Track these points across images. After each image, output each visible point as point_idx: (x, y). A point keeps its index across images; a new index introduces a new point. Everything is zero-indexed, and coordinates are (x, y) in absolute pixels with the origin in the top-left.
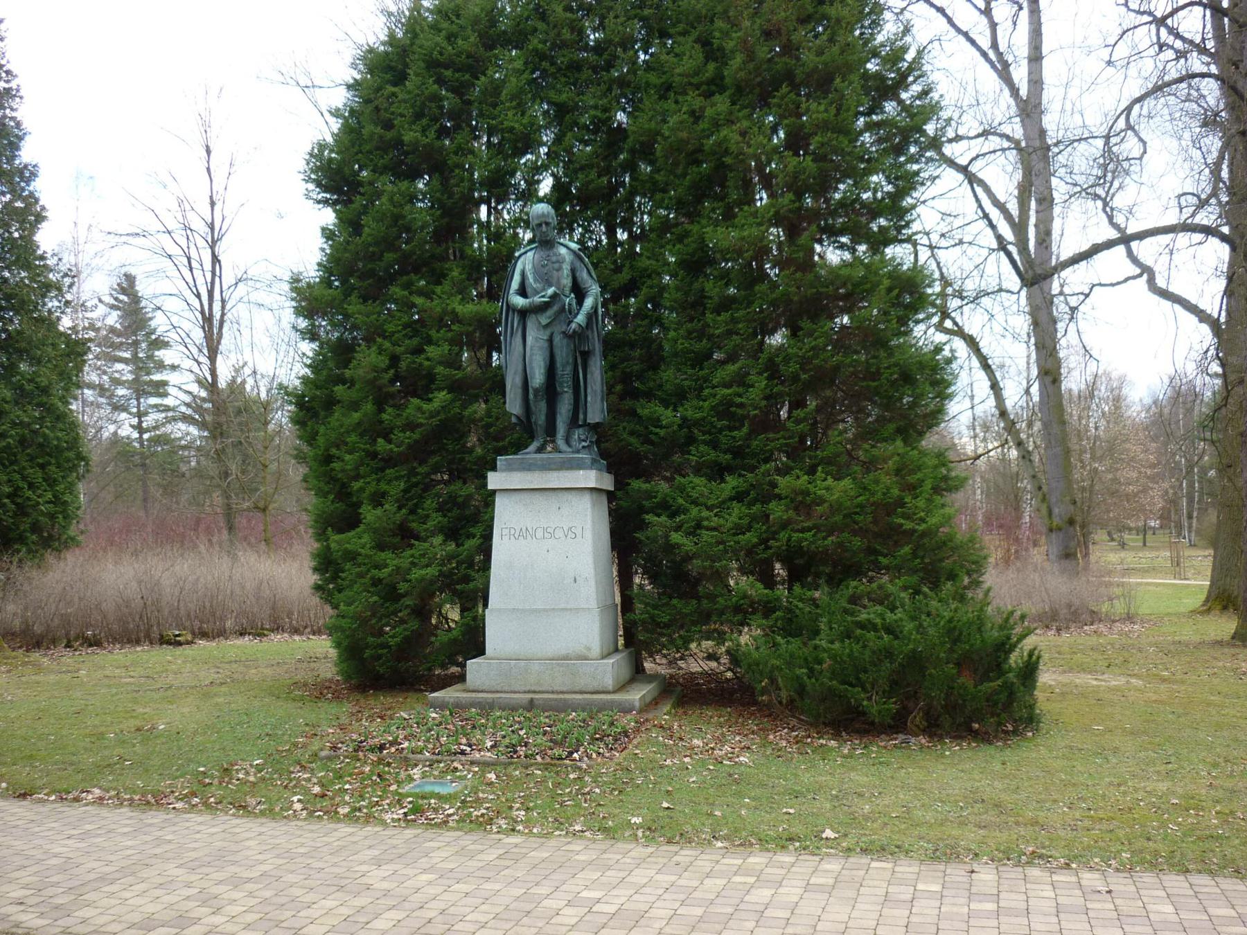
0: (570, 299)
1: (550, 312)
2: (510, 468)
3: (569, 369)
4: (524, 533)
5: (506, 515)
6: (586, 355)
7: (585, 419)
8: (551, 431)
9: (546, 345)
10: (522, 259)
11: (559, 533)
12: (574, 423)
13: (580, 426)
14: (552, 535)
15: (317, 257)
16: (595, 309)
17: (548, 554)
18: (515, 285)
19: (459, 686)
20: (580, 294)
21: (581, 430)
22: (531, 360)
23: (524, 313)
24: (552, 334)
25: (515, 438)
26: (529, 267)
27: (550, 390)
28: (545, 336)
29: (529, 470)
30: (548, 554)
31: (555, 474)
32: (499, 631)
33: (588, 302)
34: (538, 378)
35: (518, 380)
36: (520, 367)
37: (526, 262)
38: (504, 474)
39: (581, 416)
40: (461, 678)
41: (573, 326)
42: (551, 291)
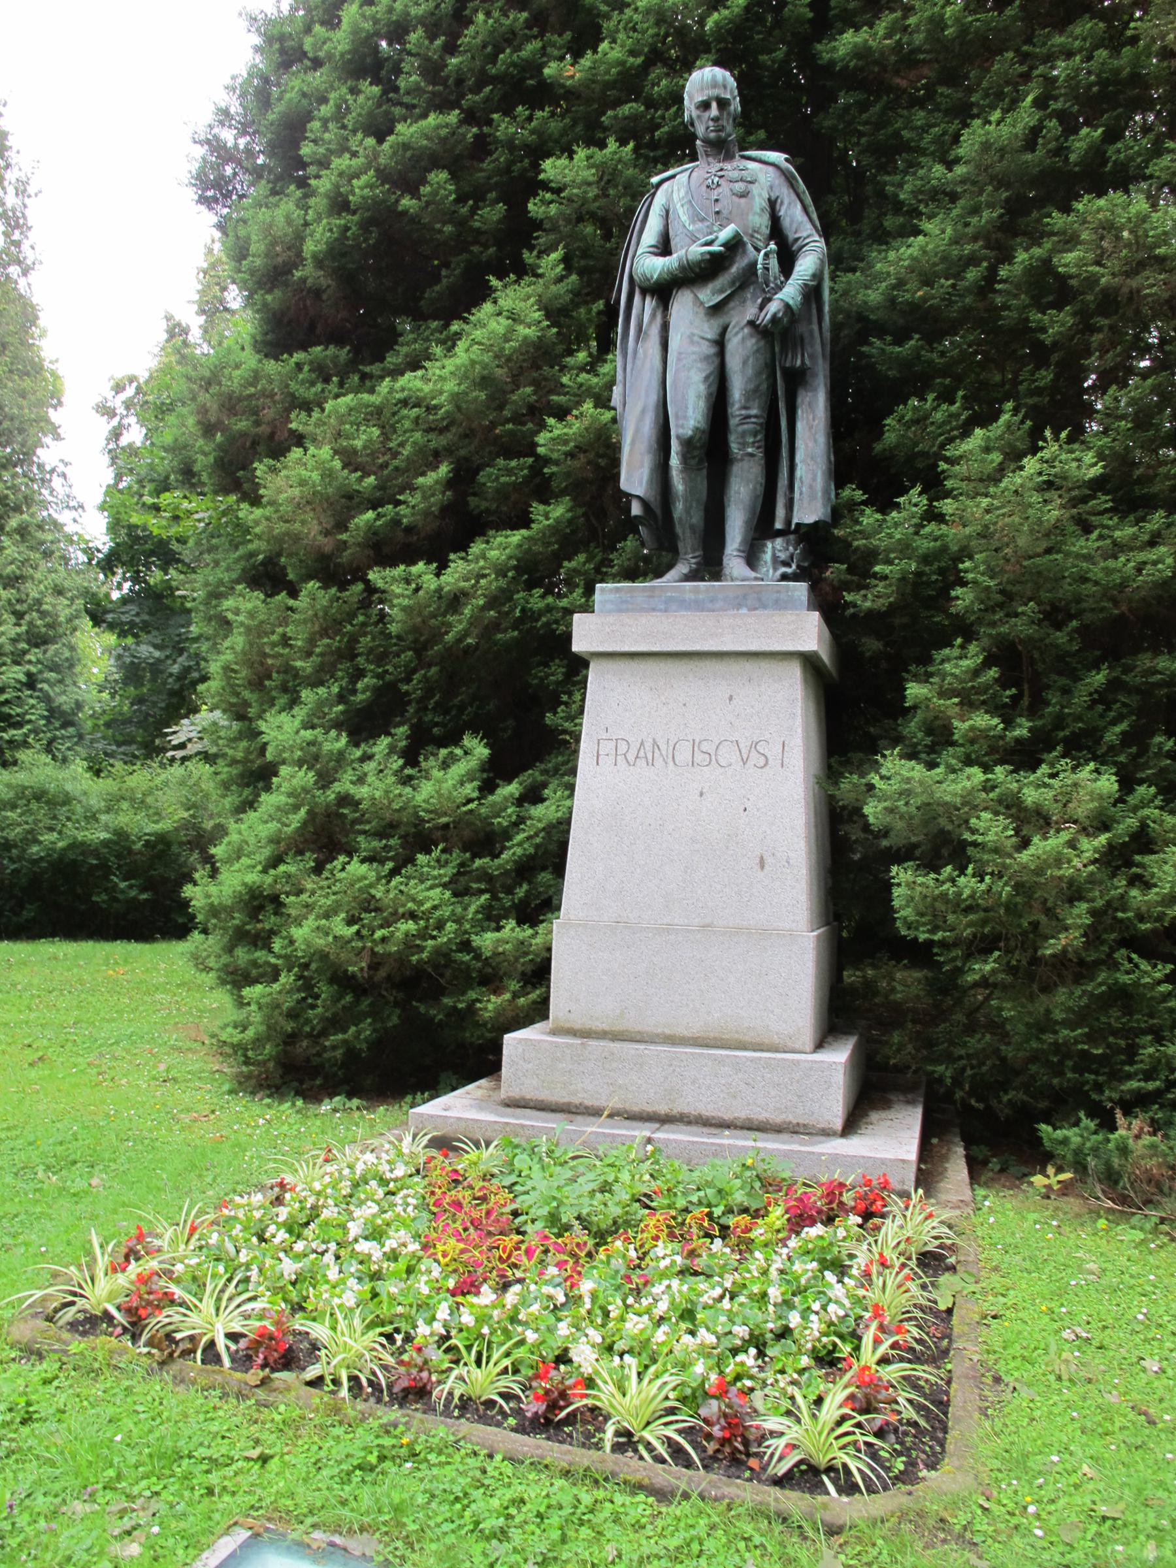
0: (764, 256)
1: (723, 280)
4: (647, 753)
5: (610, 713)
6: (796, 380)
7: (788, 521)
9: (712, 350)
10: (665, 185)
11: (728, 755)
12: (762, 527)
14: (712, 758)
15: (153, 363)
16: (817, 276)
17: (694, 769)
18: (650, 236)
20: (787, 259)
21: (779, 542)
24: (724, 330)
27: (712, 450)
28: (709, 330)
30: (694, 769)
33: (806, 265)
34: (689, 417)
35: (648, 427)
36: (653, 398)
37: (317, 1422)
38: (611, 619)
39: (780, 512)
41: (773, 307)
42: (725, 234)
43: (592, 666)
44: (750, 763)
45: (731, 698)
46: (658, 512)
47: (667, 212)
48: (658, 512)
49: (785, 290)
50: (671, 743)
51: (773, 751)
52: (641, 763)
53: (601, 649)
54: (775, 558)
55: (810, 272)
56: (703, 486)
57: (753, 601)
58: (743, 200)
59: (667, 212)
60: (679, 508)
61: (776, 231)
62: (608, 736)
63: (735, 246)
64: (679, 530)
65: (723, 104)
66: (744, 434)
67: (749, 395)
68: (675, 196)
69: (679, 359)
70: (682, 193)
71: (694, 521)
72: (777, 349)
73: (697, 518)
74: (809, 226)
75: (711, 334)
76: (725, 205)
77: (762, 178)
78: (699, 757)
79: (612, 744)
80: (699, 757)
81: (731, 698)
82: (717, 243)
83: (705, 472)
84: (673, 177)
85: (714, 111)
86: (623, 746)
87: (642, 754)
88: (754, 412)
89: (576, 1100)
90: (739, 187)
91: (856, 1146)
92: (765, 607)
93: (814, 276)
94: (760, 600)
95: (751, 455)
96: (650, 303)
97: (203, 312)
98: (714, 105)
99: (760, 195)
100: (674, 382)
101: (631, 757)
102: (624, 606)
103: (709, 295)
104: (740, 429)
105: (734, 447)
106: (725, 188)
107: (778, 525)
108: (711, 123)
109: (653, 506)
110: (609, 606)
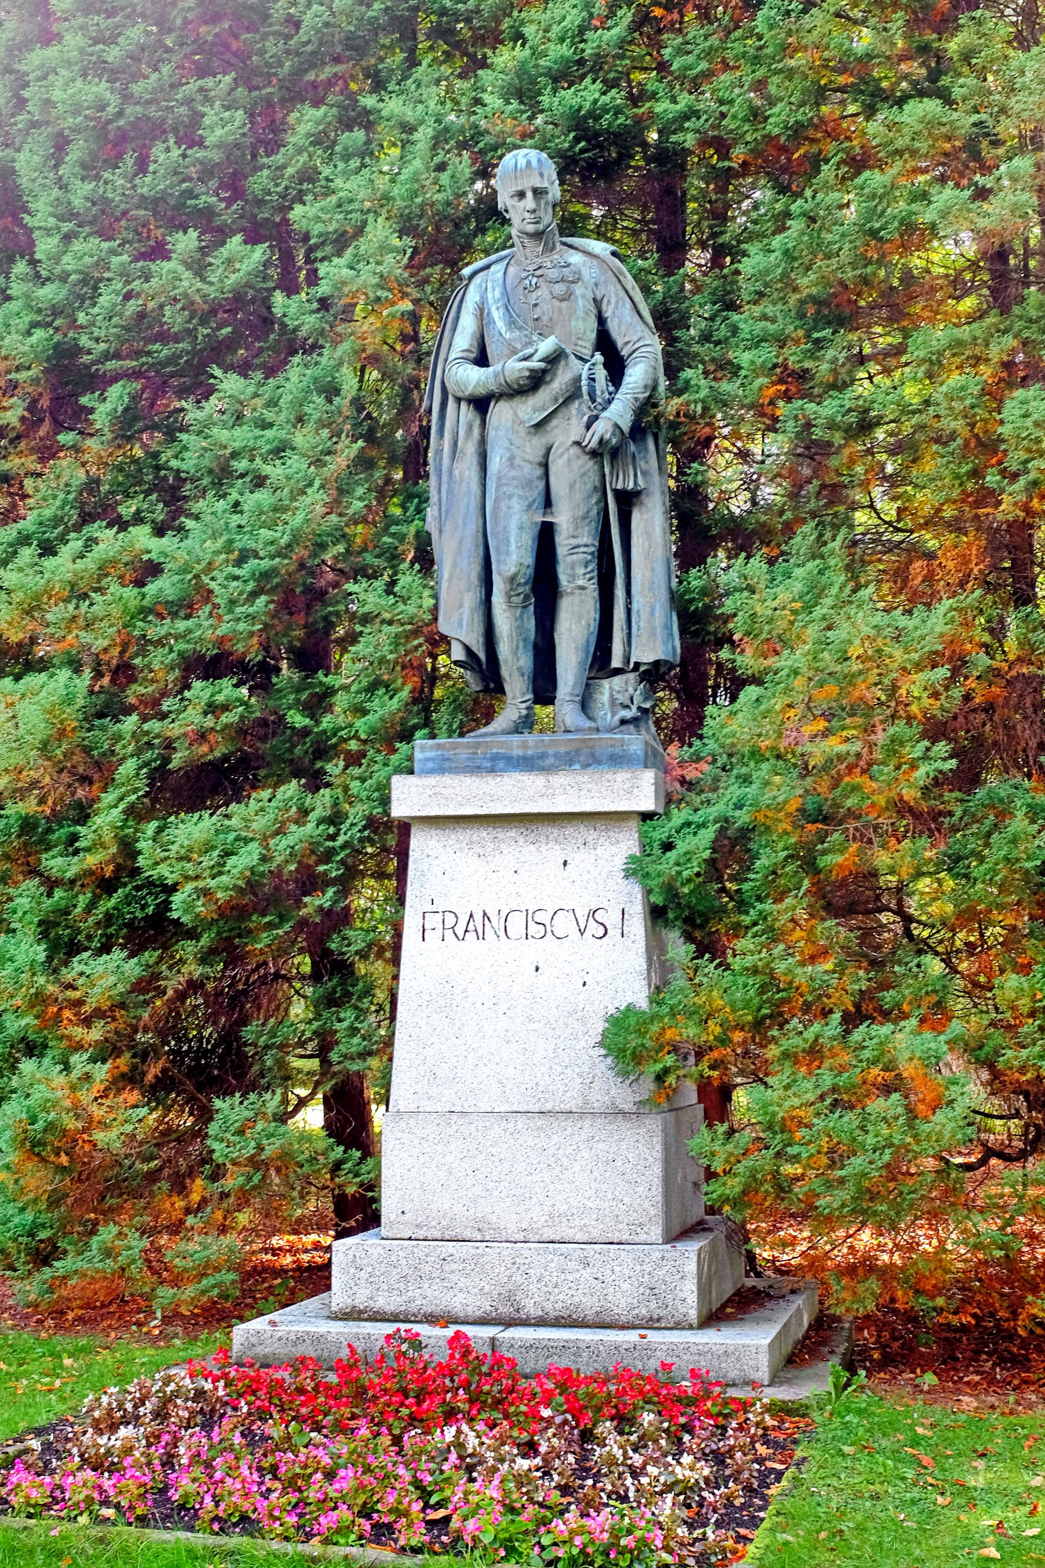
2: (443, 767)
3: (588, 538)
4: (475, 926)
8: (544, 689)
10: (478, 280)
11: (564, 924)
13: (618, 672)
18: (463, 340)
19: (313, 1304)
21: (617, 681)
22: (496, 508)
23: (481, 404)
25: (455, 699)
26: (494, 295)
28: (533, 449)
29: (492, 770)
31: (559, 779)
32: (408, 1162)
34: (515, 557)
36: (473, 525)
38: (432, 780)
40: (315, 1278)
42: (546, 346)
43: (413, 831)
44: (588, 934)
45: (565, 863)
46: (482, 656)
47: (482, 310)
48: (482, 656)
49: (613, 407)
50: (503, 915)
51: (612, 919)
52: (471, 936)
53: (423, 814)
54: (613, 700)
55: (641, 384)
56: (531, 624)
57: (585, 757)
58: (564, 304)
59: (482, 310)
60: (504, 650)
61: (605, 343)
62: (434, 908)
63: (555, 359)
64: (504, 672)
65: (539, 193)
66: (573, 566)
67: (578, 522)
68: (490, 295)
69: (499, 486)
70: (497, 294)
71: (522, 662)
72: (607, 470)
73: (526, 661)
74: (640, 326)
75: (538, 456)
76: (545, 309)
77: (585, 273)
78: (533, 929)
79: (440, 916)
80: (533, 929)
81: (565, 863)
82: (536, 357)
83: (532, 608)
84: (487, 267)
85: (529, 202)
86: (450, 921)
87: (471, 927)
88: (585, 540)
89: (413, 1308)
90: (559, 289)
91: (713, 1338)
92: (599, 762)
93: (651, 376)
94: (593, 755)
95: (583, 588)
96: (467, 413)
97: (680, 1232)
98: (529, 194)
99: (583, 296)
100: (496, 508)
101: (460, 930)
102: (447, 764)
103: (531, 409)
104: (569, 559)
105: (563, 578)
106: (543, 292)
107: (616, 663)
108: (527, 215)
109: (474, 649)
110: (430, 765)
